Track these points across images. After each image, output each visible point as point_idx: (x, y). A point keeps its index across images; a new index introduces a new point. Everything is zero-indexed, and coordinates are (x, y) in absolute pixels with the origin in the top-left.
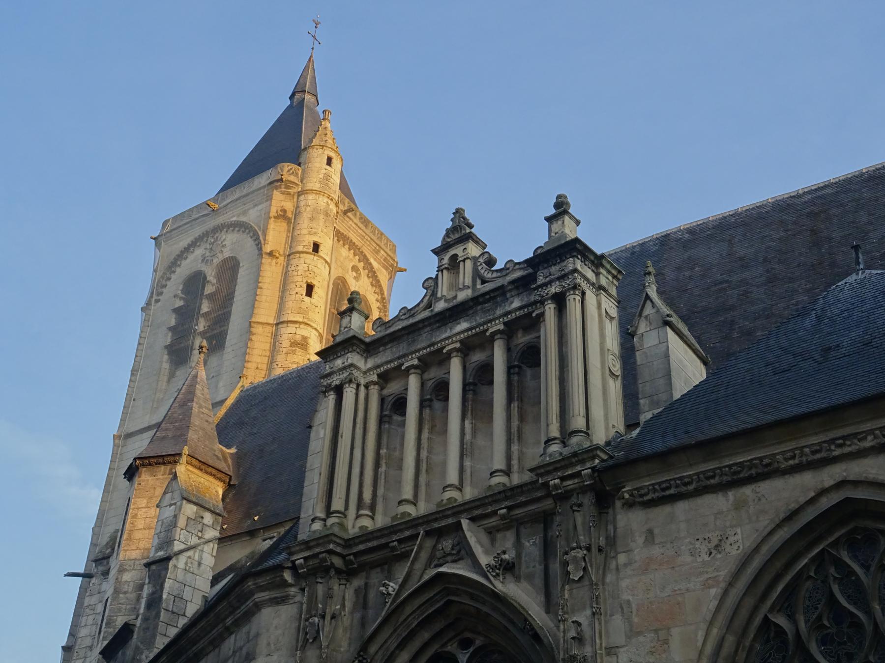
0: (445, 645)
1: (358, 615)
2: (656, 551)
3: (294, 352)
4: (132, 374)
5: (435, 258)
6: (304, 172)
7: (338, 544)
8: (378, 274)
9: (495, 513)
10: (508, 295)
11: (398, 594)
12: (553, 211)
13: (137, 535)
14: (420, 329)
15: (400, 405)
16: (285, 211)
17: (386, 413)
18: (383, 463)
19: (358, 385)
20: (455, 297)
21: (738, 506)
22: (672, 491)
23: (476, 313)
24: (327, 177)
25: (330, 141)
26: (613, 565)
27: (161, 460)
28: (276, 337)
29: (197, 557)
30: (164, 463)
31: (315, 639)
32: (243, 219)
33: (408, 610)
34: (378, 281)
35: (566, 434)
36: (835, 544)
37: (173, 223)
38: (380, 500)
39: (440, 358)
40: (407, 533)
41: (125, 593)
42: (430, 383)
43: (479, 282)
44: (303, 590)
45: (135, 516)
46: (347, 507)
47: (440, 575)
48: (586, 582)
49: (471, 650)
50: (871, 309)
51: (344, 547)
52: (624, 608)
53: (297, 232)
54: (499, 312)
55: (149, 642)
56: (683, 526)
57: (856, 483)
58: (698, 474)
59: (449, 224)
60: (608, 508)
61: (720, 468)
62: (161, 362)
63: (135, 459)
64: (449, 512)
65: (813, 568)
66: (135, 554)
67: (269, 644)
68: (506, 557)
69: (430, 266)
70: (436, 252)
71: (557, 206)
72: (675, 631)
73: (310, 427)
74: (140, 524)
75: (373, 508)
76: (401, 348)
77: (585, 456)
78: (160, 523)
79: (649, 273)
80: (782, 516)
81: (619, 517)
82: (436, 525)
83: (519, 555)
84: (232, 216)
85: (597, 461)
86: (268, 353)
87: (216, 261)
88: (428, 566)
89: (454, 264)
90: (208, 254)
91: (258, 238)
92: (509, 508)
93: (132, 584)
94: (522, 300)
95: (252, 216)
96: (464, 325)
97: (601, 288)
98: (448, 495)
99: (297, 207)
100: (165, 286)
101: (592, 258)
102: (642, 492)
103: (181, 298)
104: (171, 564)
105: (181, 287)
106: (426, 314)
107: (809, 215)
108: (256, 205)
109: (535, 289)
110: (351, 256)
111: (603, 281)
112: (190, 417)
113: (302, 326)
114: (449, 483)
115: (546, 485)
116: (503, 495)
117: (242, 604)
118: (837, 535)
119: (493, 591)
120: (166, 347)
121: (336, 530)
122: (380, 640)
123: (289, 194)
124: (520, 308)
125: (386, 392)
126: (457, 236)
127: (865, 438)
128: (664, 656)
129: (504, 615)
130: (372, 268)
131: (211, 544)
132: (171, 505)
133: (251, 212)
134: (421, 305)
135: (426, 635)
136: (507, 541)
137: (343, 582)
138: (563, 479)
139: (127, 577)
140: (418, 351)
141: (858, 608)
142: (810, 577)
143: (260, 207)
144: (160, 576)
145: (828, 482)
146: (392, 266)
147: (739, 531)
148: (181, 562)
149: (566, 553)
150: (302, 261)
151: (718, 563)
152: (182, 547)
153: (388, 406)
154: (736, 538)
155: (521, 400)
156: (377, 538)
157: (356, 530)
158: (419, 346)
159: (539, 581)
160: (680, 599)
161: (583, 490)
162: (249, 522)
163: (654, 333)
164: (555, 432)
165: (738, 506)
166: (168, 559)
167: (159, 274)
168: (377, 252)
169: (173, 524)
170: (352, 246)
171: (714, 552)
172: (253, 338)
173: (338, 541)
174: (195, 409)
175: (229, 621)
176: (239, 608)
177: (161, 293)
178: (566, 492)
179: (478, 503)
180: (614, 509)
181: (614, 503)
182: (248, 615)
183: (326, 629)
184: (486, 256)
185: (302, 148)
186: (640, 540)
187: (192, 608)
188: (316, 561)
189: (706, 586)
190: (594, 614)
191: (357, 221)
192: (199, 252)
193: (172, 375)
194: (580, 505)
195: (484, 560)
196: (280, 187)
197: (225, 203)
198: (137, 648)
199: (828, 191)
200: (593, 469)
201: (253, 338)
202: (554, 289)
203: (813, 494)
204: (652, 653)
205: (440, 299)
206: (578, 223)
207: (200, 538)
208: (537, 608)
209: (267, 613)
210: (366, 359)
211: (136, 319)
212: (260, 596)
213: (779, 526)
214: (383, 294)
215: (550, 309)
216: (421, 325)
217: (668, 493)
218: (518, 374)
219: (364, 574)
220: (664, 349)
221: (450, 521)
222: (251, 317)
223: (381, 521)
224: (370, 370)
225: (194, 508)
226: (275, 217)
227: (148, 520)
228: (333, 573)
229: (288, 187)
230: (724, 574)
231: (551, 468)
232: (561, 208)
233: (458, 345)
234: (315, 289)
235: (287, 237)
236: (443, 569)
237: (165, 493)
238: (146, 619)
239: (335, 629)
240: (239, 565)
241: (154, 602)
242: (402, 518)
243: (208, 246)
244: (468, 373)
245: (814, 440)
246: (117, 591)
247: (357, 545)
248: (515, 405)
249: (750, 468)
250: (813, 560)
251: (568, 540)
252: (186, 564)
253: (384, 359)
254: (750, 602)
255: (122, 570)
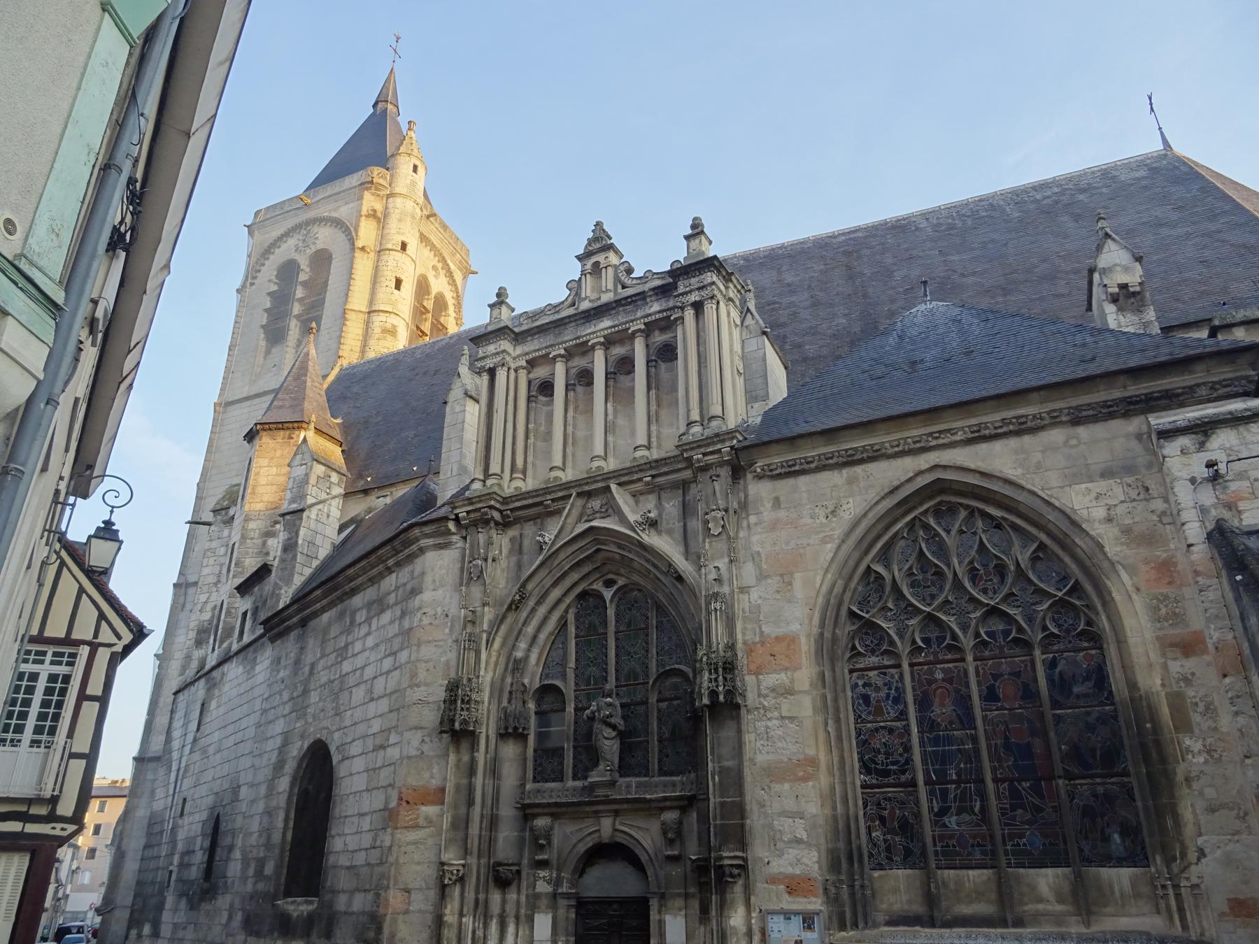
0: (591, 584)
1: (514, 559)
2: (782, 514)
3: (385, 338)
4: (230, 349)
5: (579, 264)
6: (392, 176)
7: (498, 501)
8: (454, 274)
9: (640, 480)
10: (648, 300)
11: (553, 544)
12: (689, 232)
13: (260, 490)
14: (566, 324)
15: (546, 388)
16: (375, 211)
17: (534, 393)
18: (531, 435)
19: (509, 369)
20: (599, 298)
21: (851, 481)
22: (797, 468)
23: (618, 313)
24: (413, 184)
25: (416, 150)
26: (745, 524)
27: (280, 426)
28: (368, 324)
29: (326, 510)
30: (283, 429)
31: (479, 577)
32: (334, 215)
33: (562, 555)
34: (454, 281)
35: (706, 419)
36: (926, 511)
37: (265, 214)
38: (529, 466)
39: (584, 349)
40: (560, 494)
41: (252, 539)
42: (573, 371)
43: (620, 287)
44: (465, 538)
45: (258, 474)
46: (502, 471)
47: (591, 528)
48: (724, 536)
49: (615, 588)
50: (944, 333)
51: (502, 503)
52: (756, 557)
53: (386, 231)
54: (639, 314)
55: (288, 580)
56: (805, 495)
57: (945, 467)
58: (819, 455)
59: (591, 235)
60: (739, 479)
61: (838, 451)
62: (258, 340)
63: (256, 424)
64: (599, 478)
65: (906, 530)
66: (259, 506)
67: (434, 581)
68: (652, 515)
69: (575, 270)
70: (579, 258)
71: (694, 227)
72: (798, 576)
73: (446, 403)
74: (263, 480)
75: (524, 472)
76: (548, 340)
77: (726, 437)
78: (292, 480)
79: (750, 291)
80: (887, 490)
81: (750, 487)
82: (587, 488)
83: (660, 515)
84: (324, 211)
85: (735, 441)
86: (361, 338)
87: (309, 252)
88: (579, 520)
89: (597, 269)
90: (301, 244)
91: (350, 234)
92: (653, 476)
93: (257, 531)
94: (661, 305)
95: (343, 212)
96: (606, 323)
97: (731, 300)
98: (596, 464)
99: (386, 208)
100: (259, 271)
101: (724, 273)
102: (772, 467)
103: (275, 283)
104: (305, 514)
105: (275, 273)
106: (571, 311)
107: (845, 253)
108: (347, 204)
109: (676, 296)
110: (432, 256)
111: (731, 295)
112: (305, 389)
113: (392, 315)
114: (596, 454)
115: (689, 459)
116: (648, 466)
117: (406, 548)
118: (925, 507)
119: (638, 541)
120: (263, 327)
121: (496, 489)
122: (537, 579)
123: (378, 195)
124: (660, 312)
125: (531, 376)
126: (598, 246)
127: (956, 433)
128: (788, 594)
129: (648, 561)
130: (449, 269)
131: (337, 500)
132: (302, 465)
133: (342, 209)
134: (566, 303)
135: (575, 576)
136: (650, 503)
137: (500, 532)
138: (704, 454)
139: (252, 525)
140: (566, 342)
141: (941, 561)
142: (904, 537)
143: (351, 205)
144: (295, 525)
145: (925, 466)
146: (466, 268)
147: (851, 501)
148: (313, 513)
149: (707, 514)
150: (391, 257)
151: (834, 525)
152: (314, 501)
153: (534, 388)
154: (849, 506)
155: (658, 389)
156: (533, 497)
157: (512, 490)
158: (566, 339)
159: (678, 534)
160: (801, 551)
161: (721, 464)
162: (362, 482)
163: (754, 341)
164: (695, 415)
165: (851, 481)
166: (302, 510)
167: (253, 259)
168: (454, 255)
169: (305, 480)
170: (433, 248)
171: (830, 516)
172: (348, 323)
173: (498, 498)
174: (309, 383)
175: (391, 562)
176: (401, 551)
177: (256, 278)
178: (707, 465)
179: (626, 471)
180: (745, 481)
181: (745, 475)
182: (411, 558)
183: (489, 570)
184: (626, 265)
185: (389, 154)
186: (769, 505)
187: (323, 553)
188: (478, 514)
189: (824, 541)
190: (731, 561)
191: (437, 225)
192: (292, 242)
193: (268, 352)
194: (718, 476)
195: (632, 517)
196: (370, 188)
197: (317, 199)
198: (276, 584)
199: (860, 234)
200: (732, 447)
201: (348, 323)
202: (694, 297)
203: (912, 474)
204: (778, 592)
205: (585, 299)
206: (710, 243)
207: (328, 494)
208: (678, 556)
209: (430, 556)
210: (515, 346)
211: (232, 300)
212: (425, 542)
213: (883, 498)
214: (457, 292)
215: (689, 314)
216: (567, 320)
217: (793, 469)
218: (655, 367)
219: (518, 526)
220: (761, 354)
221: (600, 485)
222: (345, 304)
223: (530, 484)
224: (519, 356)
225: (323, 468)
226: (366, 216)
227: (270, 478)
228: (492, 524)
229: (377, 189)
230: (838, 533)
231: (695, 445)
232: (697, 230)
233: (602, 340)
234: (403, 284)
235: (377, 235)
236: (595, 523)
237: (295, 454)
238: (283, 561)
239: (495, 569)
240: (359, 518)
241: (290, 547)
242: (554, 481)
243: (301, 238)
244: (610, 364)
245: (915, 433)
246: (244, 537)
247: (513, 502)
248: (653, 392)
249: (862, 453)
250: (907, 524)
251: (707, 504)
252: (317, 515)
253: (532, 348)
254: (856, 555)
255: (247, 519)
